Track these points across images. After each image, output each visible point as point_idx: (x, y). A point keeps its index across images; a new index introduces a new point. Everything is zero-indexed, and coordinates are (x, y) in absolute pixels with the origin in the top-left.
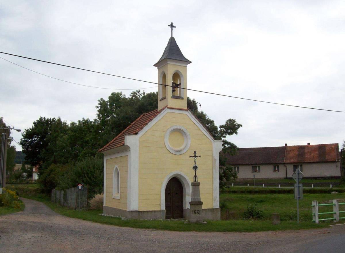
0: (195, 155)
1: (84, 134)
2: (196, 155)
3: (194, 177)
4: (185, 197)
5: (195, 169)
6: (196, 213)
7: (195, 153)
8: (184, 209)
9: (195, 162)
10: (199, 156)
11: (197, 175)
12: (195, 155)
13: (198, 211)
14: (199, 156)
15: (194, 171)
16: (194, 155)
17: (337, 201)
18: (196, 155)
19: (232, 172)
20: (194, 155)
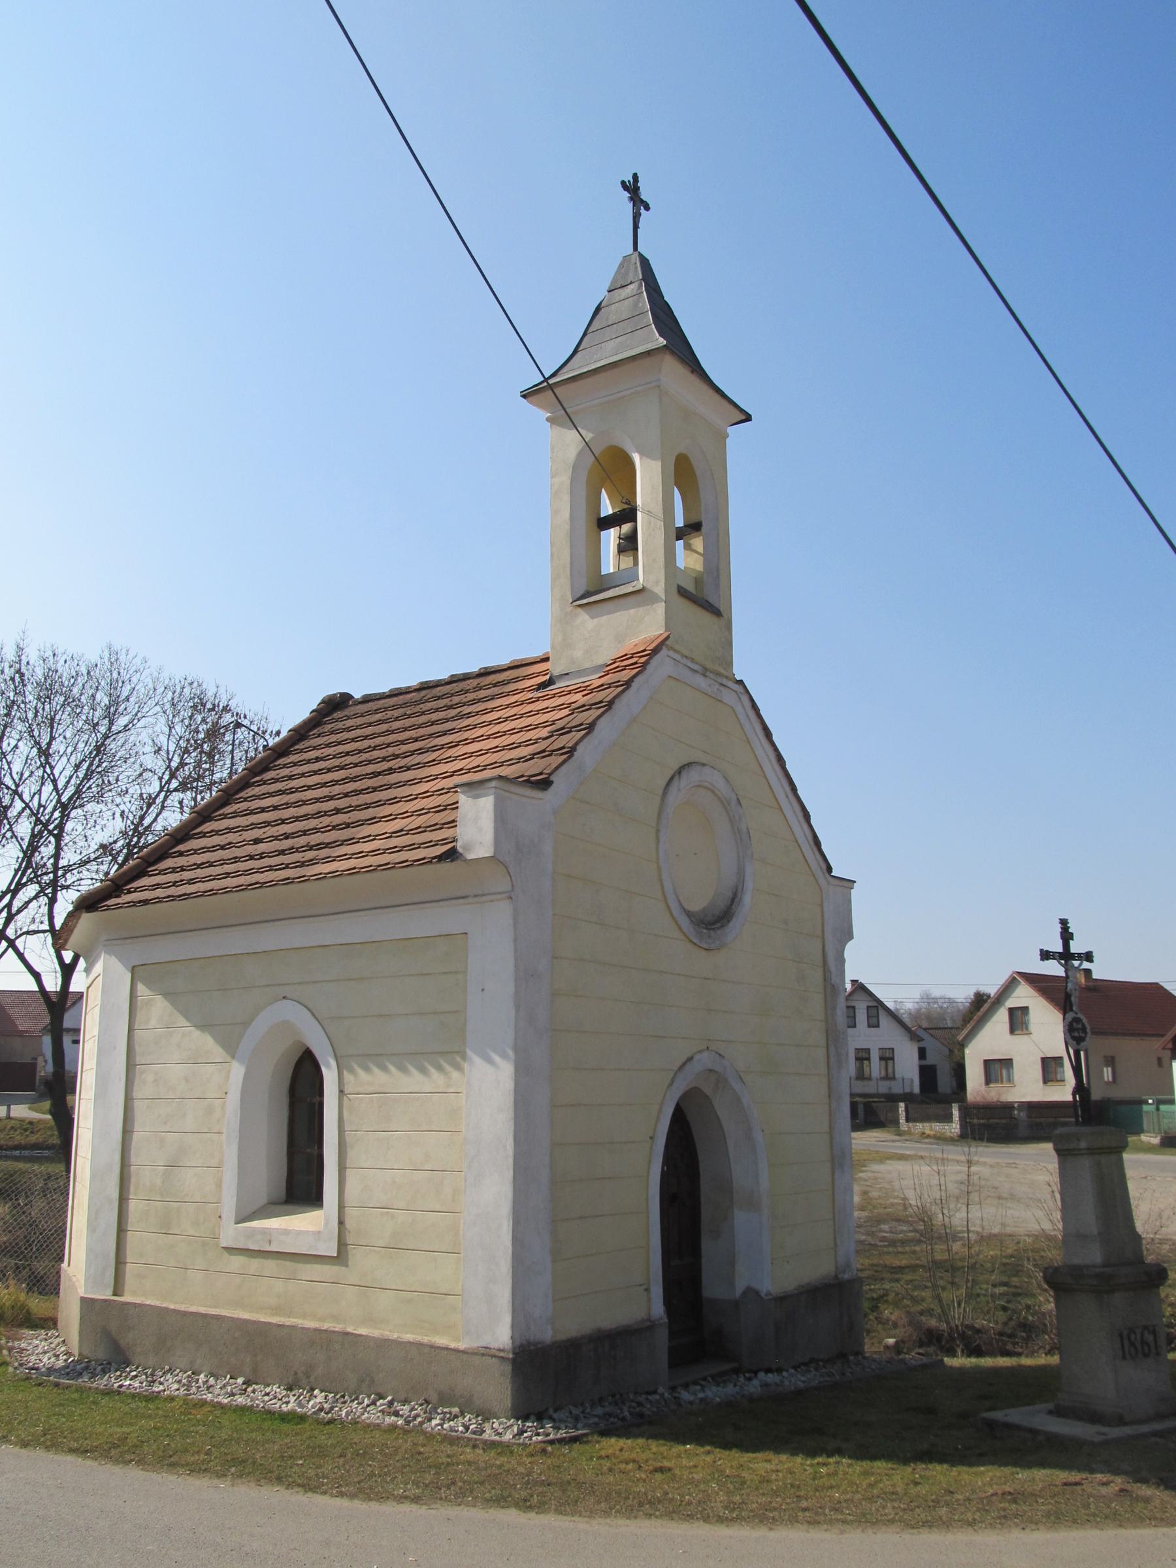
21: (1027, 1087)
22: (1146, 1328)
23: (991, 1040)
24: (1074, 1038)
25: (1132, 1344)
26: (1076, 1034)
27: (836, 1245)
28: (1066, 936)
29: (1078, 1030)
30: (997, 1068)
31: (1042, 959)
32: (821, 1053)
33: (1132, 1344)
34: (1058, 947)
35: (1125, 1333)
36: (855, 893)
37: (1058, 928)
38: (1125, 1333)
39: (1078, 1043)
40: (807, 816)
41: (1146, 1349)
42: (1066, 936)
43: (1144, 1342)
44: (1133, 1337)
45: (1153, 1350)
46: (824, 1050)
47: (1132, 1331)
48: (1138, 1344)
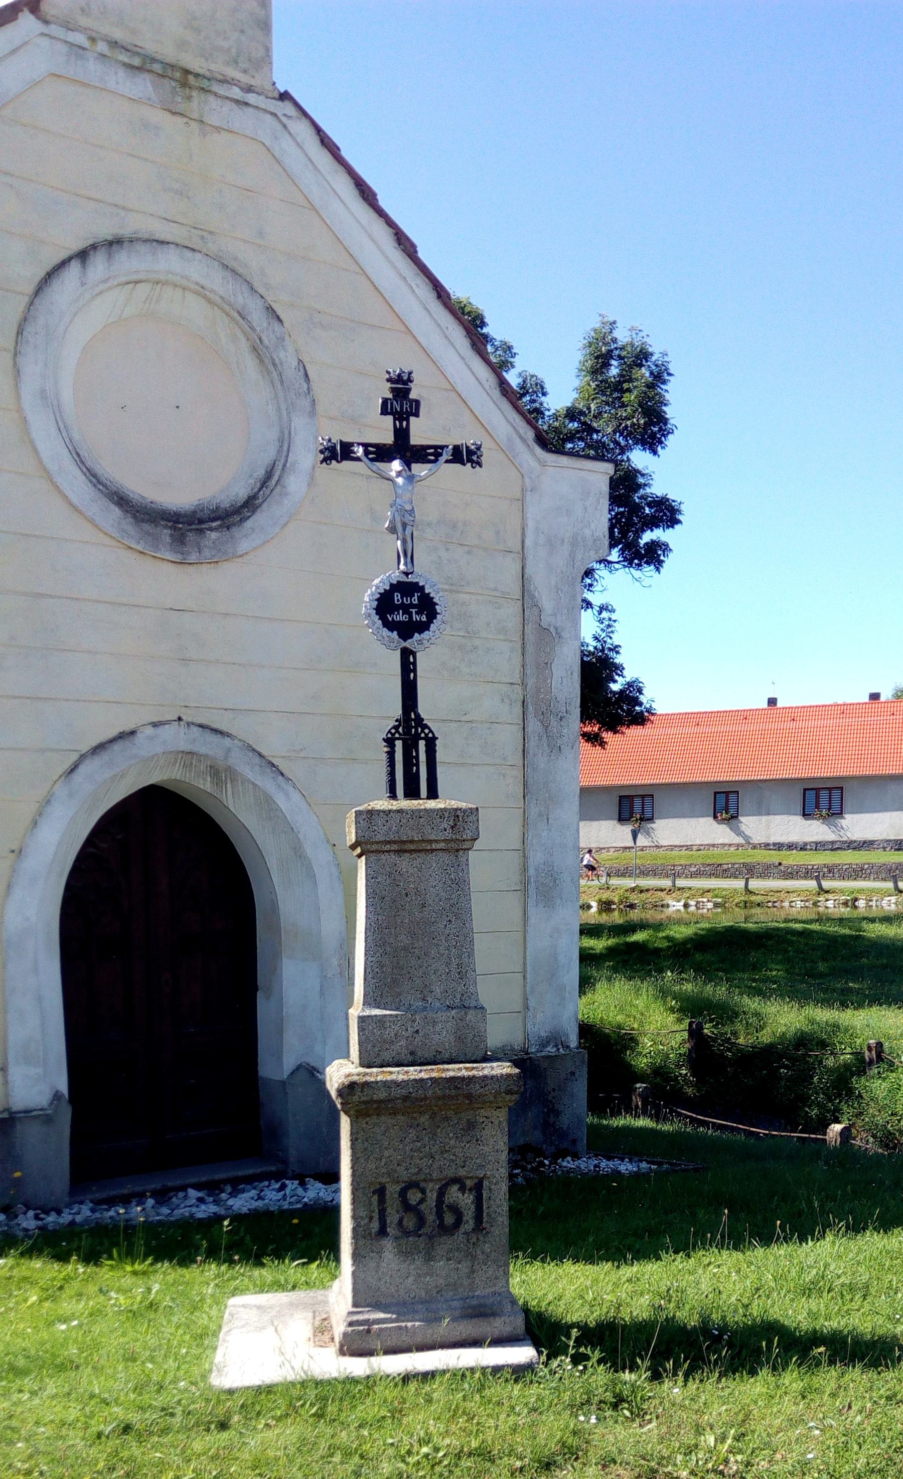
0: (402, 434)
1: (358, 1395)
2: (416, 439)
3: (390, 742)
4: (275, 969)
5: (406, 631)
6: (431, 1218)
7: (401, 402)
8: (267, 1069)
9: (403, 526)
10: (464, 456)
11: (424, 708)
12: (402, 434)
13: (454, 1194)
14: (464, 456)
15: (395, 658)
16: (387, 438)
17: (783, 1370)
18: (416, 439)
19: (136, 1451)
20: (387, 438)
22: (456, 1180)
26: (400, 617)
27: (527, 1008)
29: (406, 609)
35: (392, 1190)
38: (392, 1190)
46: (516, 730)
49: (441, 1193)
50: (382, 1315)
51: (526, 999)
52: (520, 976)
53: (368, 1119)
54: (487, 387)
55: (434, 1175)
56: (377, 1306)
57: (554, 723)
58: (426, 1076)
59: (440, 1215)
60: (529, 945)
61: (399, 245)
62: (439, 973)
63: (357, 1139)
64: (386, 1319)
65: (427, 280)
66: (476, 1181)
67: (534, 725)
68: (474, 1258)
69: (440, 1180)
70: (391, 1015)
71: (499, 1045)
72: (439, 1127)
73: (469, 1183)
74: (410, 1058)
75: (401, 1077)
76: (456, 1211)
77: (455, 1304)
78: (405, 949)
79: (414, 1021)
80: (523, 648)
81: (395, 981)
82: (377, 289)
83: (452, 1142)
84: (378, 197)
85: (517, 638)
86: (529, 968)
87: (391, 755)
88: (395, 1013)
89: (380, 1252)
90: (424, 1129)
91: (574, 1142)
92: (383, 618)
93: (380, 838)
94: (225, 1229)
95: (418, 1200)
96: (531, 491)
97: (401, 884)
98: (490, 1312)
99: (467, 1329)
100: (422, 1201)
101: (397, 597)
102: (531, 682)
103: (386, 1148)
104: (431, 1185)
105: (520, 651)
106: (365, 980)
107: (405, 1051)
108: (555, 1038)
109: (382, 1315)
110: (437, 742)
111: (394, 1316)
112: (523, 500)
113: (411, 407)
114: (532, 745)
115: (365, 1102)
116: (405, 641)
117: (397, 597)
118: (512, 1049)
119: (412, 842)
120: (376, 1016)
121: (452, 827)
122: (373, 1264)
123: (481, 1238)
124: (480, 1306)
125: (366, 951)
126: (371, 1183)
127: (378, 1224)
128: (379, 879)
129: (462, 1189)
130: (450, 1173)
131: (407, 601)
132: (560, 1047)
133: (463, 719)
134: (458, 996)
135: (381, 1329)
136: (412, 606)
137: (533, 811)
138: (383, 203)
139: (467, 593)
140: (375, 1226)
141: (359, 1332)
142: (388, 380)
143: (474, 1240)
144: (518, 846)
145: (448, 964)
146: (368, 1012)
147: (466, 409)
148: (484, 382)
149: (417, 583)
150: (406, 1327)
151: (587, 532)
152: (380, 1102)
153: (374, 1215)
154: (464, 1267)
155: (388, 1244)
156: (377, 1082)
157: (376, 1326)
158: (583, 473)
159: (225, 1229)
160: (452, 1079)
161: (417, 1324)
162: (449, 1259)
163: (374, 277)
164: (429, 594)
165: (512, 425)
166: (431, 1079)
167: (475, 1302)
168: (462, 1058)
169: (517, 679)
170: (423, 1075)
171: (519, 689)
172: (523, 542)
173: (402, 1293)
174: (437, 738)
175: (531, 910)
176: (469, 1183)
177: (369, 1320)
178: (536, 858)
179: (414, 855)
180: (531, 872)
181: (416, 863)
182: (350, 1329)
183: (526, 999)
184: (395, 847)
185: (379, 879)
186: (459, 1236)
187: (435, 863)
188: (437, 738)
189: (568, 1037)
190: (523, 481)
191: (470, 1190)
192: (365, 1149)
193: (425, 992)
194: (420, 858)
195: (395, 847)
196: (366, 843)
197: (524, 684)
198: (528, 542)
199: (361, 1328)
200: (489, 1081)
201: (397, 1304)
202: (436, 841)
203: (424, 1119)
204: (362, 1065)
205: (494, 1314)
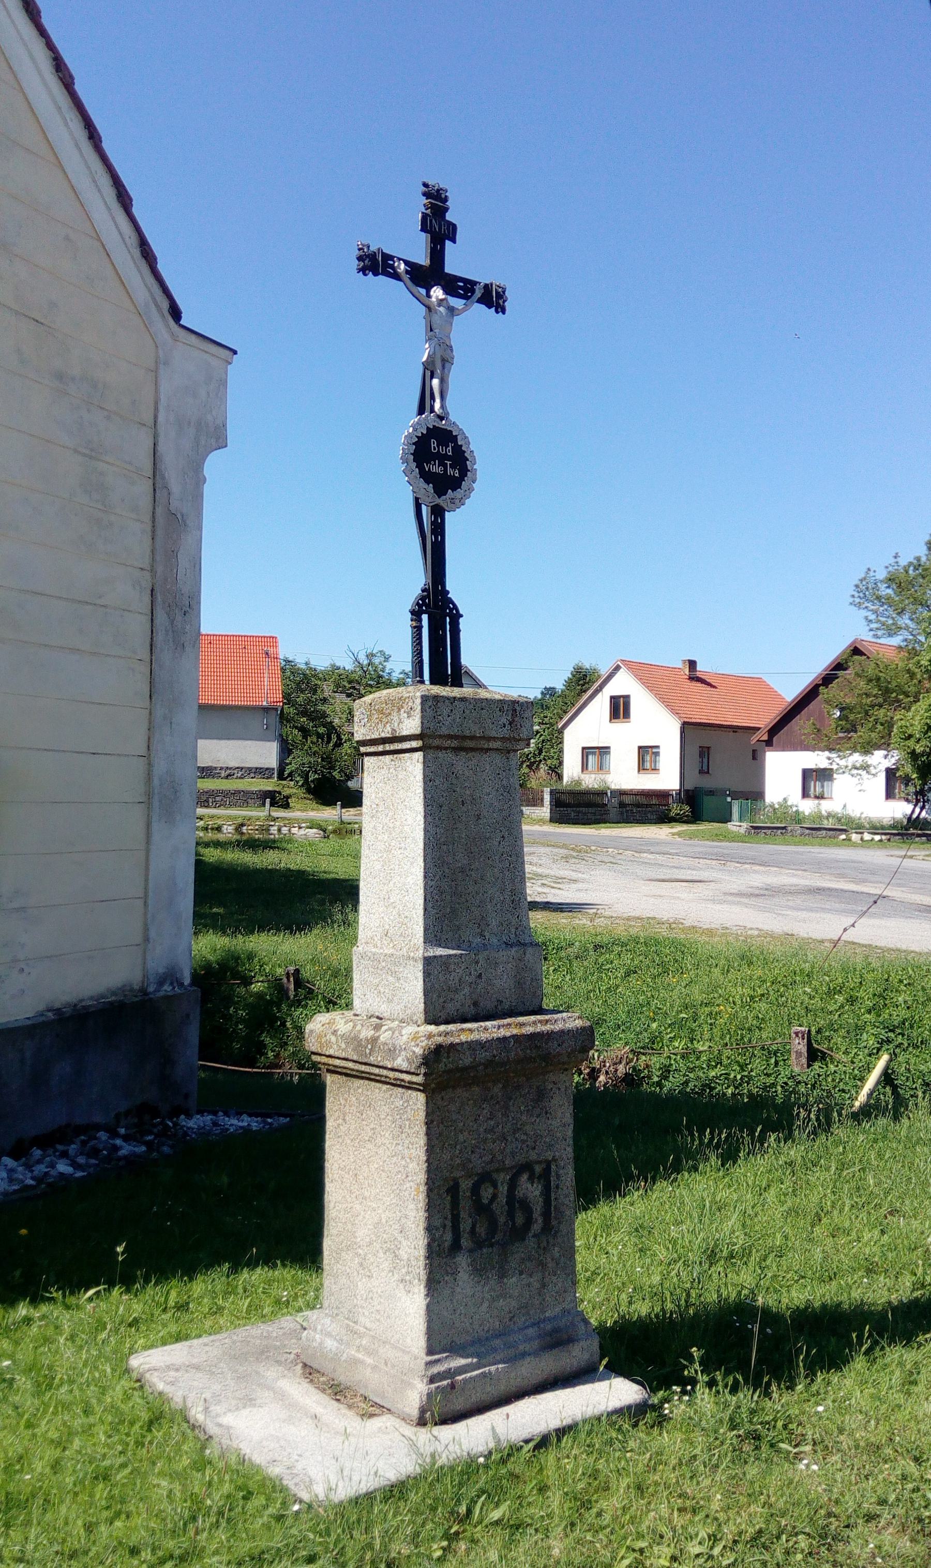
3: (416, 614)
20: (422, 258)
21: (623, 776)
22: (527, 1167)
23: (588, 726)
24: (426, 476)
25: (481, 1209)
26: (436, 468)
27: (147, 939)
28: (438, 226)
29: (442, 458)
30: (596, 754)
31: (363, 270)
32: (137, 625)
33: (481, 1209)
34: (417, 251)
35: (466, 1185)
36: (236, 371)
37: (419, 205)
38: (466, 1185)
39: (440, 492)
40: (124, 199)
41: (520, 1220)
42: (438, 226)
43: (516, 1203)
44: (486, 1193)
45: (537, 1227)
46: (146, 619)
47: (485, 1178)
48: (500, 1208)
49: (513, 1185)
50: (462, 1362)
51: (146, 929)
52: (140, 903)
53: (443, 1094)
54: (129, 244)
55: (507, 1162)
56: (454, 1349)
57: (179, 618)
58: (508, 1034)
59: (511, 1215)
60: (151, 868)
61: (57, 71)
62: (495, 902)
63: (432, 1121)
64: (467, 1365)
65: (80, 117)
66: (544, 1166)
67: (161, 617)
68: (542, 1265)
69: (511, 1168)
70: (455, 955)
71: (119, 985)
72: (510, 1099)
73: (538, 1169)
74: (472, 1011)
75: (484, 1036)
76: (525, 1206)
77: (531, 1332)
78: (462, 871)
79: (477, 963)
80: (153, 532)
81: (453, 911)
82: (32, 110)
83: (524, 1118)
84: (42, 14)
85: (147, 518)
86: (151, 894)
87: (418, 629)
88: (460, 952)
89: (455, 1273)
90: (498, 1102)
91: (186, 1096)
92: (420, 466)
93: (444, 731)
94: (120, 1259)
95: (490, 1197)
96: (164, 364)
97: (458, 789)
98: (565, 1337)
99: (548, 1364)
100: (494, 1196)
101: (434, 443)
102: (160, 569)
103: (461, 1131)
104: (502, 1175)
105: (150, 533)
106: (425, 910)
107: (469, 1002)
108: (170, 976)
109: (462, 1362)
110: (461, 620)
111: (475, 1360)
112: (156, 371)
113: (448, 229)
114: (159, 638)
115: (449, 1072)
116: (439, 497)
117: (434, 443)
118: (132, 990)
119: (473, 738)
120: (441, 956)
121: (510, 724)
122: (447, 1292)
123: (551, 1240)
124: (556, 1330)
125: (425, 872)
126: (446, 1180)
127: (451, 1235)
128: (437, 782)
129: (531, 1179)
130: (520, 1159)
131: (443, 451)
132: (175, 984)
133: (99, 602)
134: (513, 930)
135: (465, 1380)
136: (446, 457)
137: (159, 712)
138: (45, 21)
139: (107, 463)
140: (448, 1237)
141: (444, 1388)
142: (424, 194)
143: (545, 1244)
144: (143, 752)
145: (502, 891)
146: (431, 953)
147: (110, 265)
148: (127, 239)
149: (451, 432)
150: (490, 1373)
151: (209, 417)
152: (465, 1069)
153: (446, 1222)
154: (535, 1281)
155: (463, 1261)
156: (462, 1044)
157: (459, 1378)
158: (207, 356)
159: (120, 1259)
160: (533, 1036)
161: (500, 1366)
162: (521, 1273)
163: (30, 97)
164: (461, 446)
165: (149, 291)
166: (513, 1036)
167: (549, 1327)
168: (521, 1009)
169: (146, 564)
170: (503, 1033)
171: (147, 575)
172: (156, 417)
173: (476, 1327)
174: (462, 616)
175: (155, 826)
176: (538, 1169)
177: (450, 1369)
178: (160, 767)
179: (470, 755)
180: (156, 782)
181: (475, 761)
182: (433, 1386)
183: (146, 929)
184: (455, 743)
185: (437, 782)
186: (531, 1242)
187: (490, 763)
188: (462, 616)
189: (182, 974)
190: (157, 352)
191: (539, 1178)
192: (440, 1134)
193: (482, 923)
194: (476, 758)
195: (455, 743)
196: (430, 737)
197: (153, 571)
198: (161, 419)
199: (445, 1383)
200: (566, 1037)
201: (473, 1343)
202: (495, 739)
203: (497, 1090)
204: (431, 1019)
205: (571, 1340)
